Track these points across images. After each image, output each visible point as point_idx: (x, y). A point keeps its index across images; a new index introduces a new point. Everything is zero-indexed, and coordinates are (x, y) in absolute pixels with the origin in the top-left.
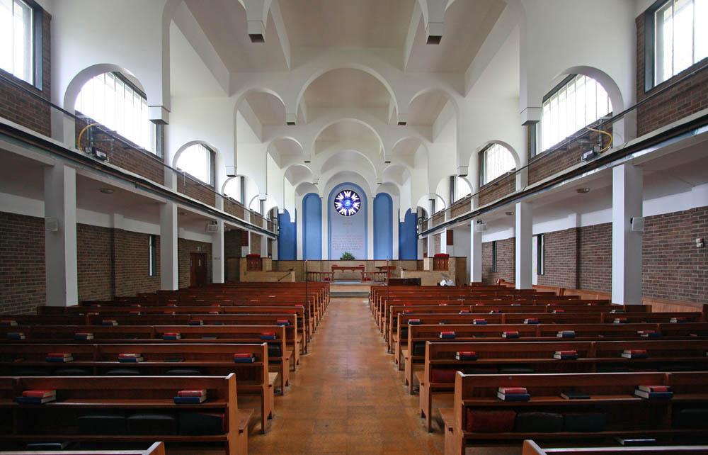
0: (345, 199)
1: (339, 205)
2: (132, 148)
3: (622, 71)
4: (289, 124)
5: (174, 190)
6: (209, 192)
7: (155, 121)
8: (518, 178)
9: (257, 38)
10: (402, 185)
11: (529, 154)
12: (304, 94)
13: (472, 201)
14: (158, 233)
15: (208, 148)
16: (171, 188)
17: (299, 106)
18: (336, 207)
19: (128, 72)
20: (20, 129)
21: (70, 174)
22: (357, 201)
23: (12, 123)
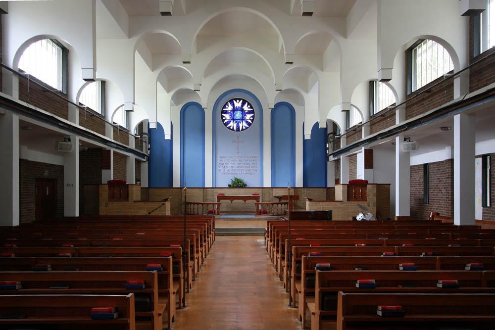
0: (235, 109)
1: (227, 117)
4: (164, 14)
6: (59, 100)
8: (457, 83)
11: (406, 92)
18: (223, 121)
22: (249, 112)
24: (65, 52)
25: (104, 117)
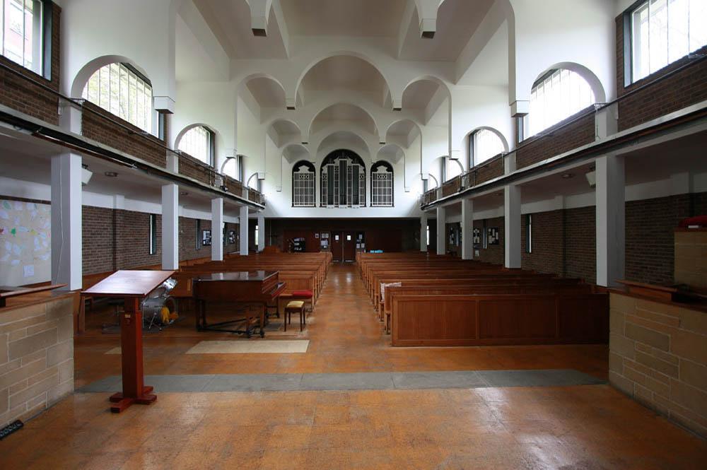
3: (602, 69)
4: (289, 108)
5: (247, 200)
6: (208, 172)
8: (507, 161)
9: (259, 32)
10: (454, 82)
11: (425, 190)
12: (302, 82)
13: (438, 192)
14: (159, 212)
15: (206, 128)
17: (272, 10)
19: (137, 64)
21: (176, 187)
24: (212, 136)
25: (241, 183)
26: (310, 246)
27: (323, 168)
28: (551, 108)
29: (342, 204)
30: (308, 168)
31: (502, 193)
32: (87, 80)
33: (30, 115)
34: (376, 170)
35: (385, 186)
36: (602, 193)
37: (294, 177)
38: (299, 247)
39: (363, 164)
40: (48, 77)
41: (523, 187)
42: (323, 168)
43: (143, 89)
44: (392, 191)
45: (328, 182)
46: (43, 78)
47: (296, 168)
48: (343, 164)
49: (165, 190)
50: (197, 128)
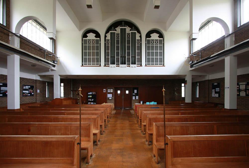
2: (42, 50)
7: (51, 39)
10: (166, 30)
16: (13, 44)
20: (24, 52)
21: (17, 58)
23: (42, 60)
26: (99, 99)
27: (106, 35)
28: (205, 38)
29: (122, 64)
30: (95, 35)
31: (223, 61)
32: (22, 26)
33: (30, 53)
34: (150, 37)
35: (153, 56)
36: (229, 72)
37: (84, 43)
38: (91, 98)
39: (139, 32)
40: (5, 24)
41: (238, 57)
42: (106, 35)
43: (35, 26)
44: (162, 54)
45: (111, 46)
46: (3, 25)
47: (85, 35)
48: (123, 31)
49: (9, 58)
50: (30, 21)
